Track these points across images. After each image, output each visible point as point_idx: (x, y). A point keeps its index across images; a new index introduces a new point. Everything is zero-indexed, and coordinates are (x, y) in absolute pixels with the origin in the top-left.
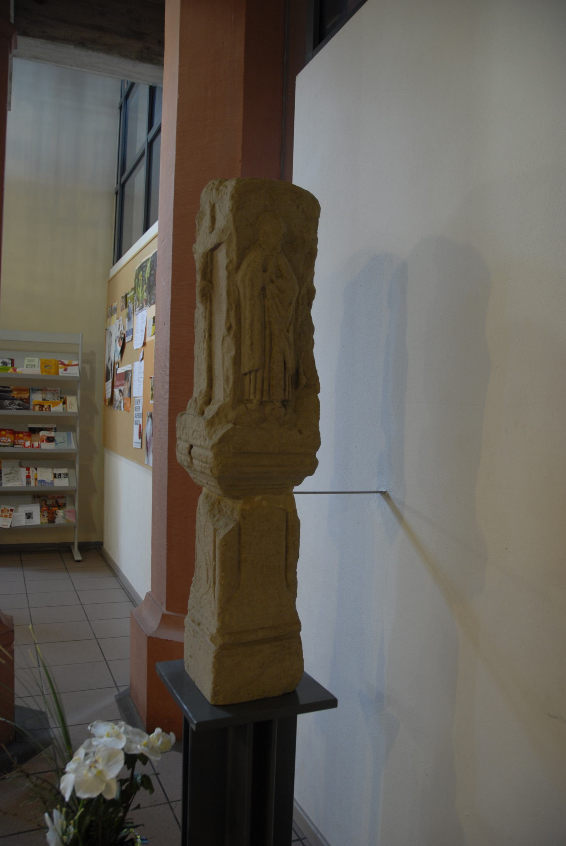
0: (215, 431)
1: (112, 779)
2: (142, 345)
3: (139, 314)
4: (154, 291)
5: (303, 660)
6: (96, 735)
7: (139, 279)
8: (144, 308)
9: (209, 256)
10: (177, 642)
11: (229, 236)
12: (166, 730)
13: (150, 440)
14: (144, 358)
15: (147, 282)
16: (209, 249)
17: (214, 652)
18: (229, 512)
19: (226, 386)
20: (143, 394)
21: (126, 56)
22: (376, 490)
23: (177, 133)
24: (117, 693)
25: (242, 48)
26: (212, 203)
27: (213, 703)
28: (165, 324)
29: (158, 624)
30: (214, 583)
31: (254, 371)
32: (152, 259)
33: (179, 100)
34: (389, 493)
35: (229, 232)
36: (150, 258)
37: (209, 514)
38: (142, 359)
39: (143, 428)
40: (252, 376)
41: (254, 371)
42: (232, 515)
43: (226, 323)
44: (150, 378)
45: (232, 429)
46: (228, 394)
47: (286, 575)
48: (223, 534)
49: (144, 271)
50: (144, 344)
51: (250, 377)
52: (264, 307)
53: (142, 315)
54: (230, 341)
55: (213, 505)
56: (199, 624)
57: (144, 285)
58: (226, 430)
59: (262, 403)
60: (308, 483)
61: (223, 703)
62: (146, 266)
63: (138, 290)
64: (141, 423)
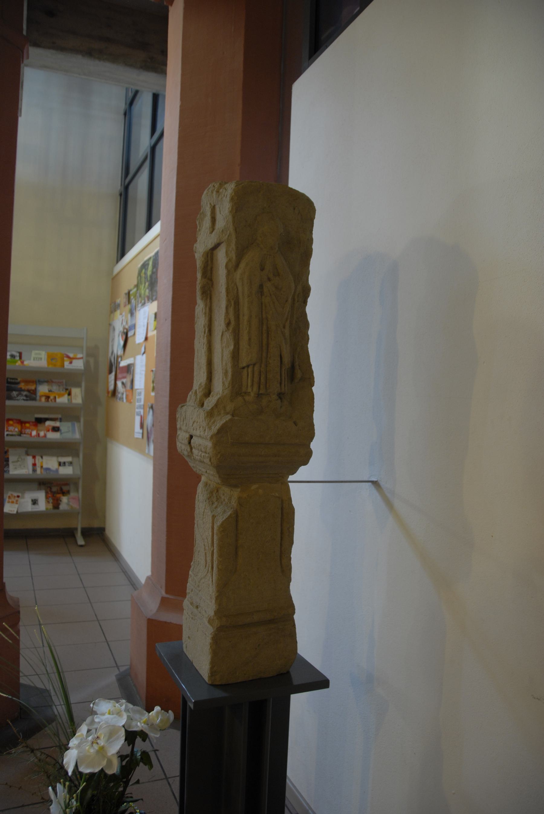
0: (214, 422)
1: (113, 755)
2: (144, 339)
5: (297, 642)
6: (98, 712)
8: (146, 304)
11: (229, 236)
12: (165, 709)
13: (151, 430)
16: (209, 249)
17: (211, 634)
18: (226, 500)
19: (225, 379)
21: (131, 66)
24: (117, 672)
26: (213, 205)
27: (210, 683)
31: (251, 365)
37: (207, 501)
38: (144, 353)
41: (251, 365)
42: (230, 503)
43: (225, 319)
45: (230, 420)
46: (227, 386)
47: (281, 560)
50: (146, 339)
52: (262, 304)
54: (228, 336)
55: (211, 493)
59: (259, 396)
60: (302, 473)
61: (217, 683)
62: (148, 264)
64: (142, 414)
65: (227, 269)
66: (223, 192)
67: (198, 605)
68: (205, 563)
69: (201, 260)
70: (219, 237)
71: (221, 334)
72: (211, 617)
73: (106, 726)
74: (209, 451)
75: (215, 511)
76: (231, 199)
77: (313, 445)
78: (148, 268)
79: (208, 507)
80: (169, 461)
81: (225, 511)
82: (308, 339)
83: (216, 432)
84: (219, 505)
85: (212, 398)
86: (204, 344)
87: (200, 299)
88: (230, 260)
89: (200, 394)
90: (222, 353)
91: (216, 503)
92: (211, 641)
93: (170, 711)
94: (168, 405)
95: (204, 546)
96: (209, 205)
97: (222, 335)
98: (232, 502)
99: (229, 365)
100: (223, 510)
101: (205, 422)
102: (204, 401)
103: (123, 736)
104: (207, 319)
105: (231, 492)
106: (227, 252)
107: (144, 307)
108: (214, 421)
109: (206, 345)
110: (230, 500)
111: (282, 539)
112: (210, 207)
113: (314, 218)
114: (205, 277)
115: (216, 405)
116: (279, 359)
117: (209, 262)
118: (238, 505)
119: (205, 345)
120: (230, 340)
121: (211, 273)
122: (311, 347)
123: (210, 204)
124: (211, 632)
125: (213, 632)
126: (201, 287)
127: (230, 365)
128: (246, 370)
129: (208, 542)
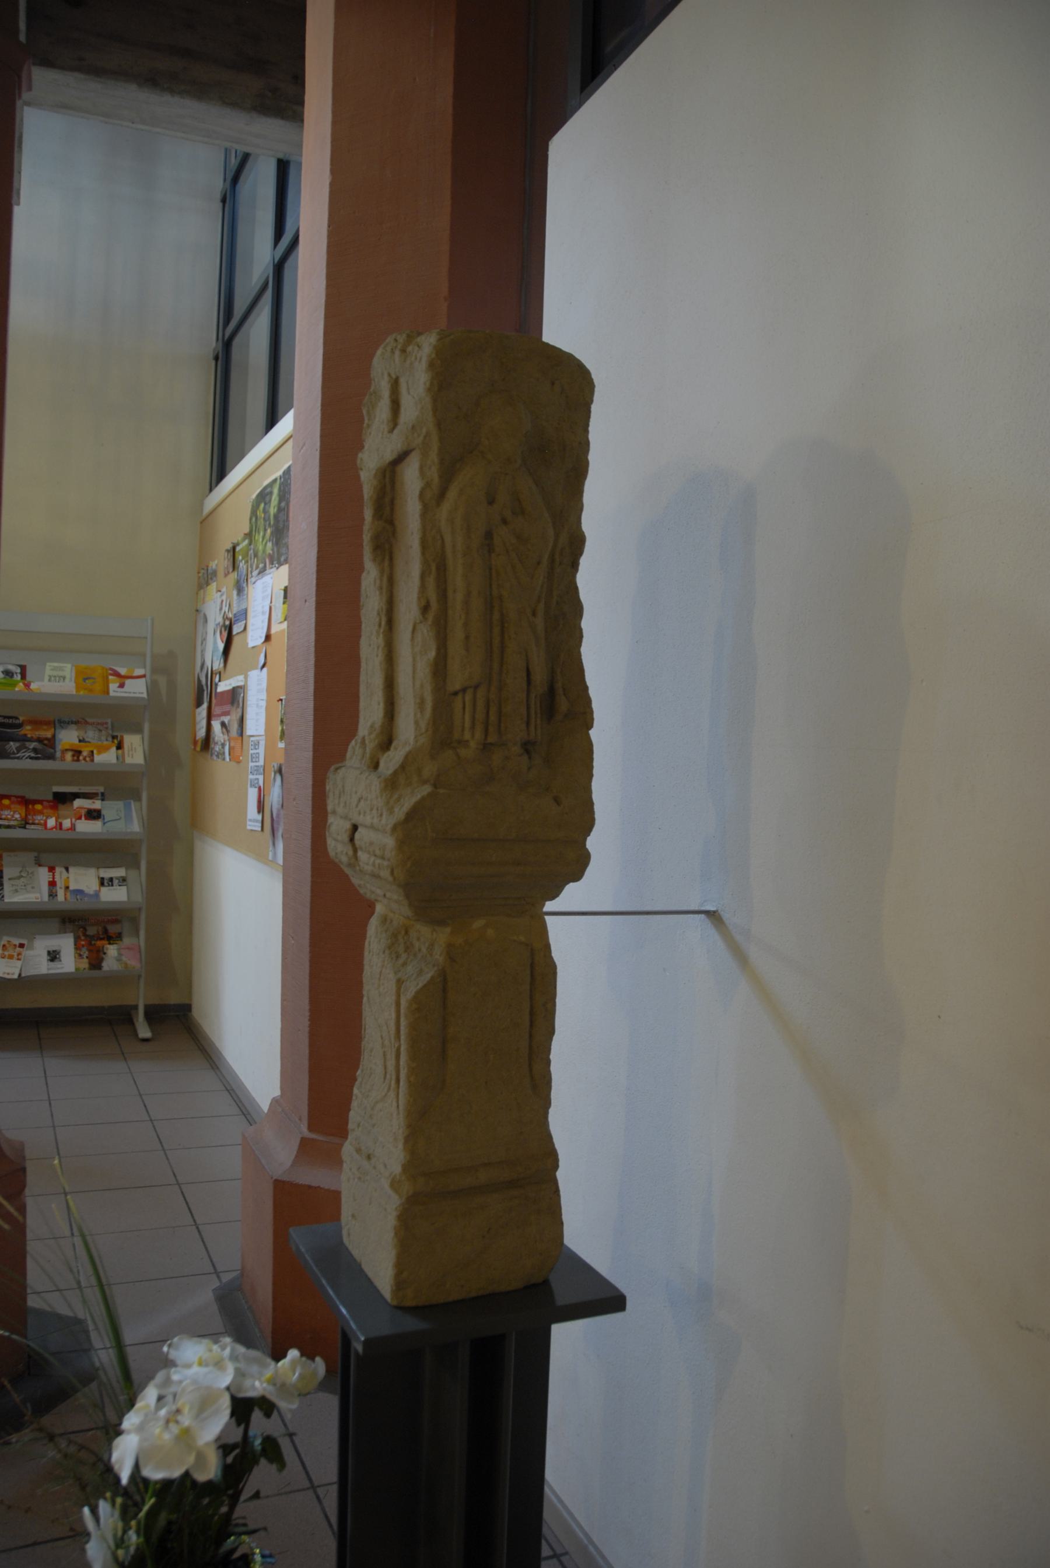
0: (398, 800)
1: (207, 1444)
2: (263, 639)
3: (259, 581)
4: (286, 540)
5: (562, 1223)
6: (179, 1362)
7: (259, 517)
8: (267, 572)
9: (388, 475)
10: (328, 1191)
11: (425, 437)
12: (308, 1353)
13: (278, 815)
14: (267, 664)
15: (272, 523)
16: (387, 462)
17: (396, 1209)
18: (424, 950)
19: (419, 715)
20: (266, 730)
21: (234, 105)
22: (697, 908)
23: (329, 246)
24: (218, 1284)
25: (449, 90)
26: (394, 377)
27: (395, 1303)
28: (306, 601)
29: (293, 1157)
30: (398, 1081)
31: (471, 687)
32: (282, 480)
33: (332, 185)
34: (722, 913)
35: (424, 430)
36: (279, 478)
37: (387, 952)
38: (264, 666)
39: (265, 793)
40: (468, 697)
41: (471, 687)
42: (431, 955)
43: (419, 599)
44: (278, 701)
45: (430, 795)
46: (423, 730)
47: (530, 1065)
48: (415, 990)
49: (267, 502)
50: (268, 638)
51: (464, 698)
52: (490, 569)
53: (263, 583)
54: (426, 632)
55: (395, 936)
56: (369, 1157)
57: (267, 528)
58: (419, 797)
59: (486, 747)
60: (572, 895)
61: (413, 1303)
62: (271, 493)
63: (256, 538)
64: (261, 783)
128: (460, 697)
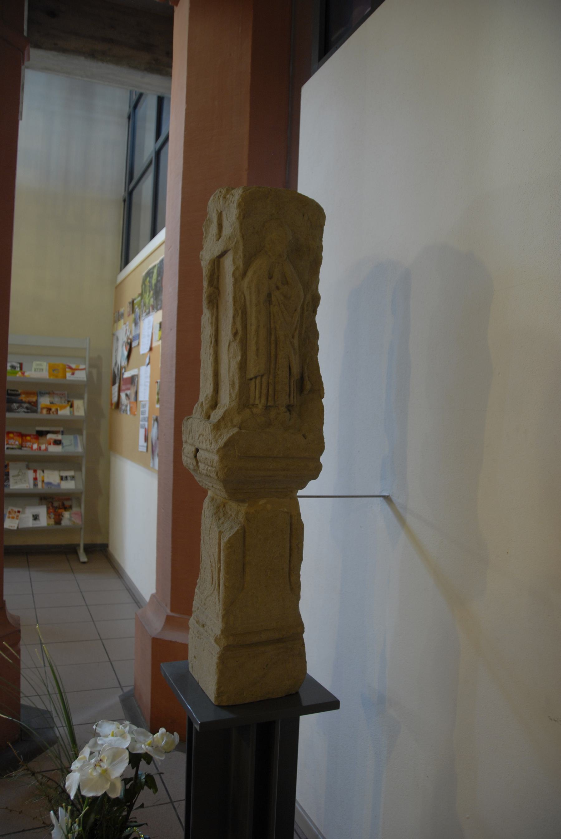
0: (220, 435)
1: (116, 778)
2: (148, 349)
5: (306, 662)
6: (101, 734)
8: (151, 313)
11: (236, 243)
12: (170, 730)
13: (155, 443)
16: (216, 256)
17: (218, 653)
18: (233, 516)
19: (232, 390)
21: (135, 68)
24: (121, 693)
26: (220, 211)
27: (217, 704)
31: (259, 376)
37: (214, 516)
38: (148, 364)
41: (259, 376)
42: (237, 518)
43: (232, 329)
45: (237, 433)
46: (234, 398)
47: (289, 577)
50: (151, 349)
52: (270, 313)
54: (235, 346)
55: (218, 508)
59: (267, 408)
60: (312, 487)
61: (224, 704)
62: (153, 272)
64: (146, 426)
65: (234, 277)
66: (230, 198)
67: (204, 624)
68: (211, 581)
69: (207, 268)
70: (226, 244)
71: (228, 344)
72: (217, 636)
73: (110, 749)
74: (216, 464)
75: (222, 527)
76: (238, 205)
77: (323, 459)
78: (152, 277)
79: (214, 523)
80: (174, 476)
81: (232, 527)
82: (318, 349)
83: (223, 445)
84: (226, 520)
85: (218, 411)
86: (210, 355)
87: (206, 308)
88: (237, 268)
89: (206, 406)
90: (229, 364)
91: (223, 519)
92: (217, 661)
93: (175, 733)
94: (173, 417)
95: (211, 562)
96: (215, 211)
97: (229, 346)
98: (239, 517)
99: (237, 376)
100: (230, 526)
101: (211, 435)
102: (210, 414)
103: (127, 759)
104: (214, 329)
105: (238, 507)
106: (234, 260)
107: (148, 317)
108: (221, 434)
109: (212, 356)
110: (238, 515)
111: (290, 556)
112: (217, 214)
113: (324, 225)
114: (212, 286)
115: (223, 418)
116: (288, 370)
117: (216, 270)
118: (246, 520)
119: (211, 356)
120: (238, 350)
121: (218, 281)
122: (321, 358)
123: (217, 210)
124: (217, 652)
125: (219, 652)
126: (207, 296)
127: (237, 376)
128: (253, 381)
129: (214, 559)
